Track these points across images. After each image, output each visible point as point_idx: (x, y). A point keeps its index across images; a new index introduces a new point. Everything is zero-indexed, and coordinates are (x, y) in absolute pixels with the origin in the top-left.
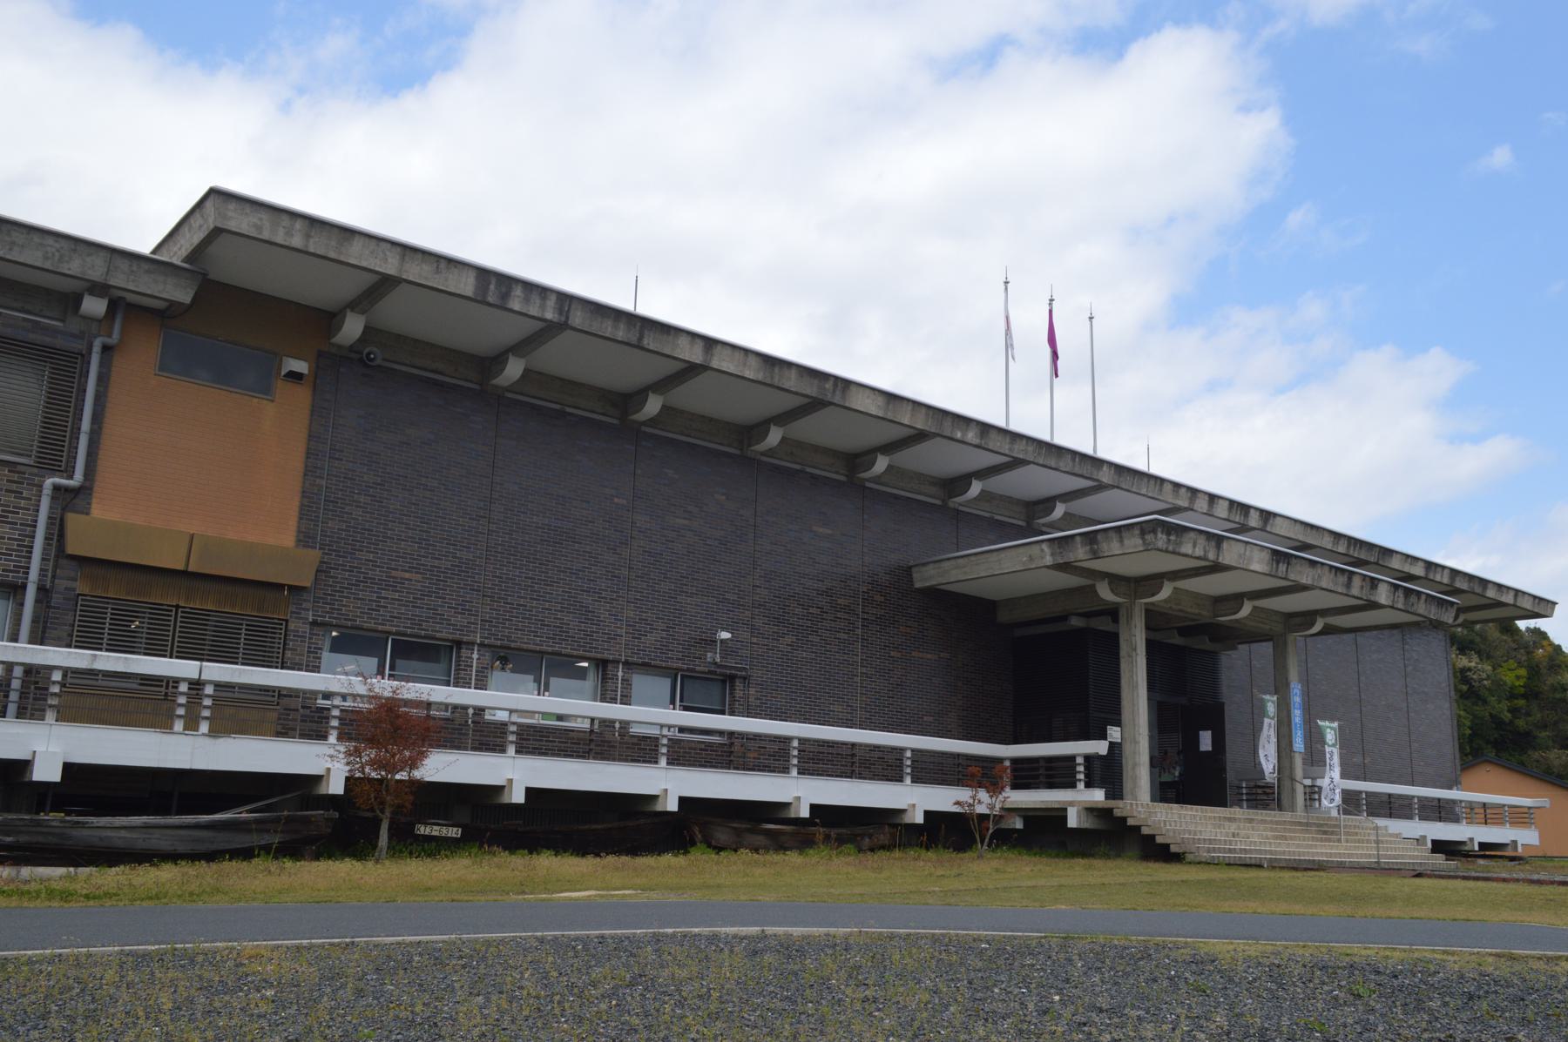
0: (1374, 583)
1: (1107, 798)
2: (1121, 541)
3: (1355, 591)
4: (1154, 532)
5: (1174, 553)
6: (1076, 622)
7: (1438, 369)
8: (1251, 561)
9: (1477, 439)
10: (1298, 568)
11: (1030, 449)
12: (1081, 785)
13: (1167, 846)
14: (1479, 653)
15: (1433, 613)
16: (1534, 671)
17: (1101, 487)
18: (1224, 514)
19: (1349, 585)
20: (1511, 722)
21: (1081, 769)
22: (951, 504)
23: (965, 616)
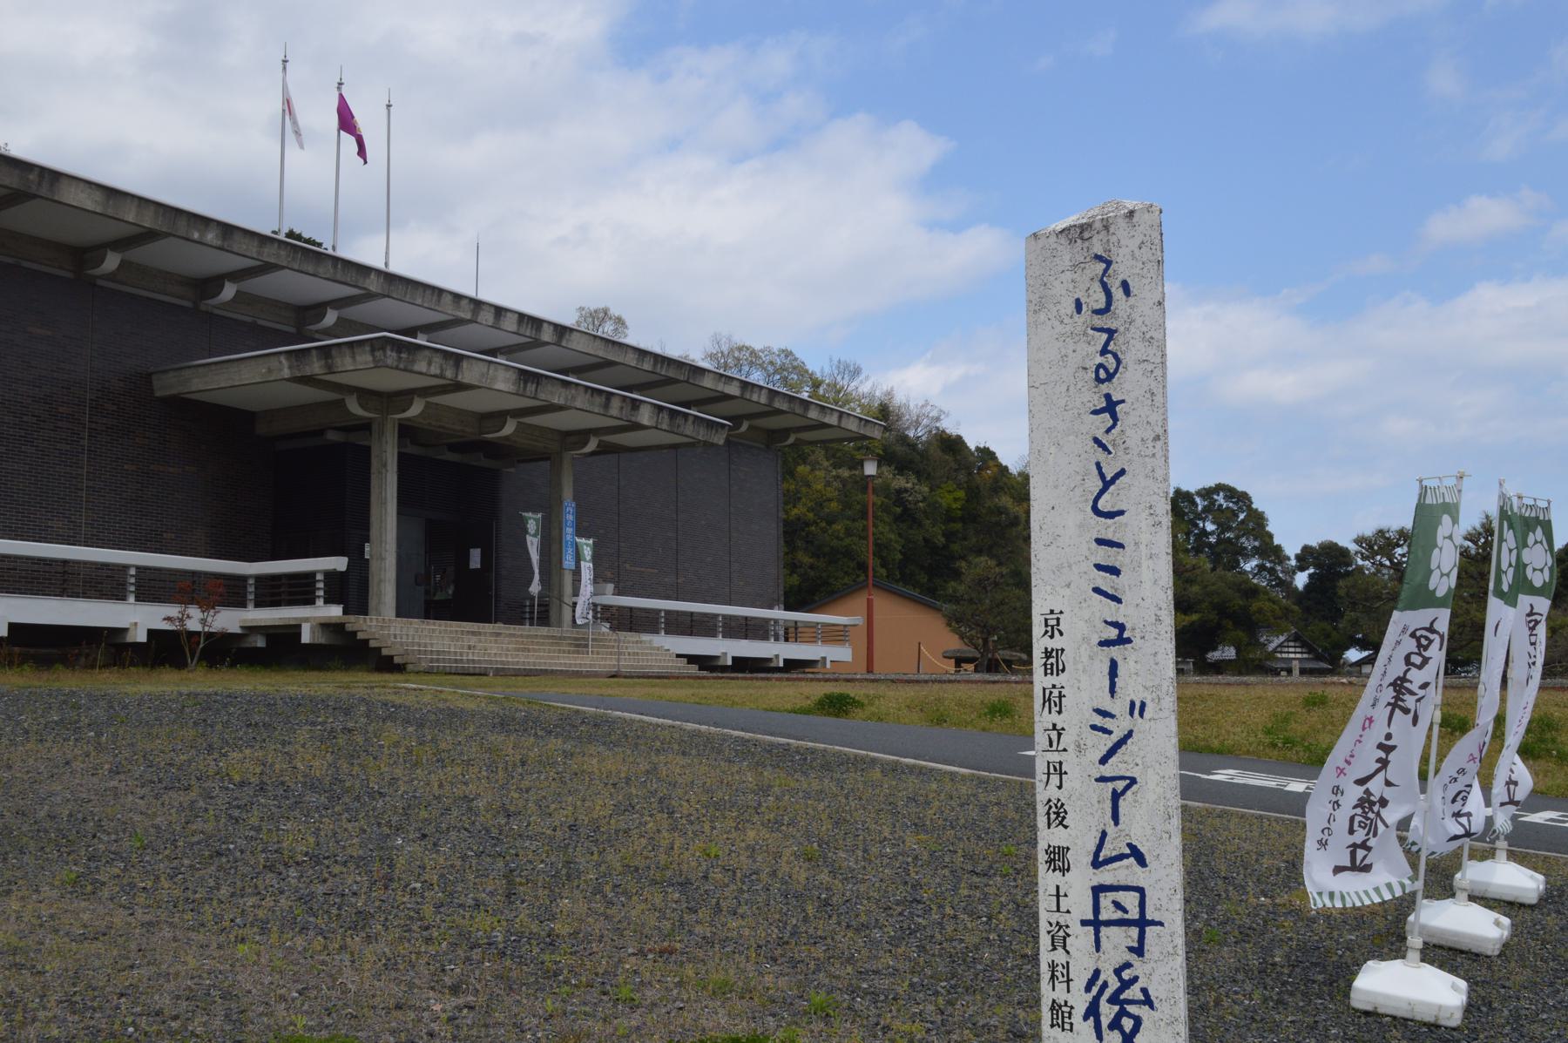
0: (636, 405)
1: (345, 613)
2: (353, 357)
3: (614, 411)
4: (383, 349)
5: (405, 370)
6: (332, 436)
7: (914, 146)
8: (495, 384)
9: (957, 227)
10: (550, 388)
11: (283, 253)
12: (320, 602)
13: (392, 657)
14: (918, 474)
15: (702, 434)
16: (973, 493)
17: (369, 296)
18: (513, 328)
19: (607, 406)
20: (945, 547)
21: (321, 585)
22: (203, 308)
23: (222, 427)
